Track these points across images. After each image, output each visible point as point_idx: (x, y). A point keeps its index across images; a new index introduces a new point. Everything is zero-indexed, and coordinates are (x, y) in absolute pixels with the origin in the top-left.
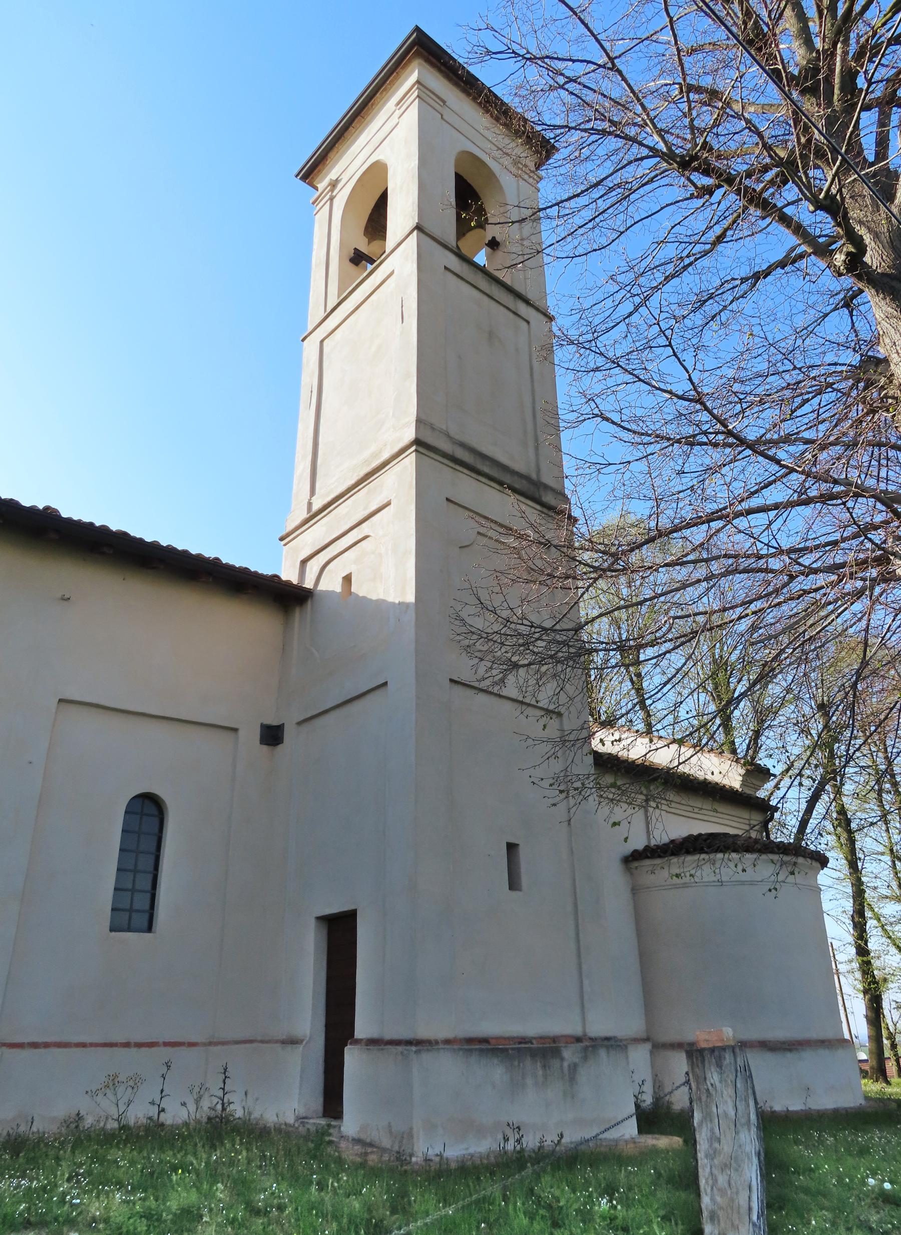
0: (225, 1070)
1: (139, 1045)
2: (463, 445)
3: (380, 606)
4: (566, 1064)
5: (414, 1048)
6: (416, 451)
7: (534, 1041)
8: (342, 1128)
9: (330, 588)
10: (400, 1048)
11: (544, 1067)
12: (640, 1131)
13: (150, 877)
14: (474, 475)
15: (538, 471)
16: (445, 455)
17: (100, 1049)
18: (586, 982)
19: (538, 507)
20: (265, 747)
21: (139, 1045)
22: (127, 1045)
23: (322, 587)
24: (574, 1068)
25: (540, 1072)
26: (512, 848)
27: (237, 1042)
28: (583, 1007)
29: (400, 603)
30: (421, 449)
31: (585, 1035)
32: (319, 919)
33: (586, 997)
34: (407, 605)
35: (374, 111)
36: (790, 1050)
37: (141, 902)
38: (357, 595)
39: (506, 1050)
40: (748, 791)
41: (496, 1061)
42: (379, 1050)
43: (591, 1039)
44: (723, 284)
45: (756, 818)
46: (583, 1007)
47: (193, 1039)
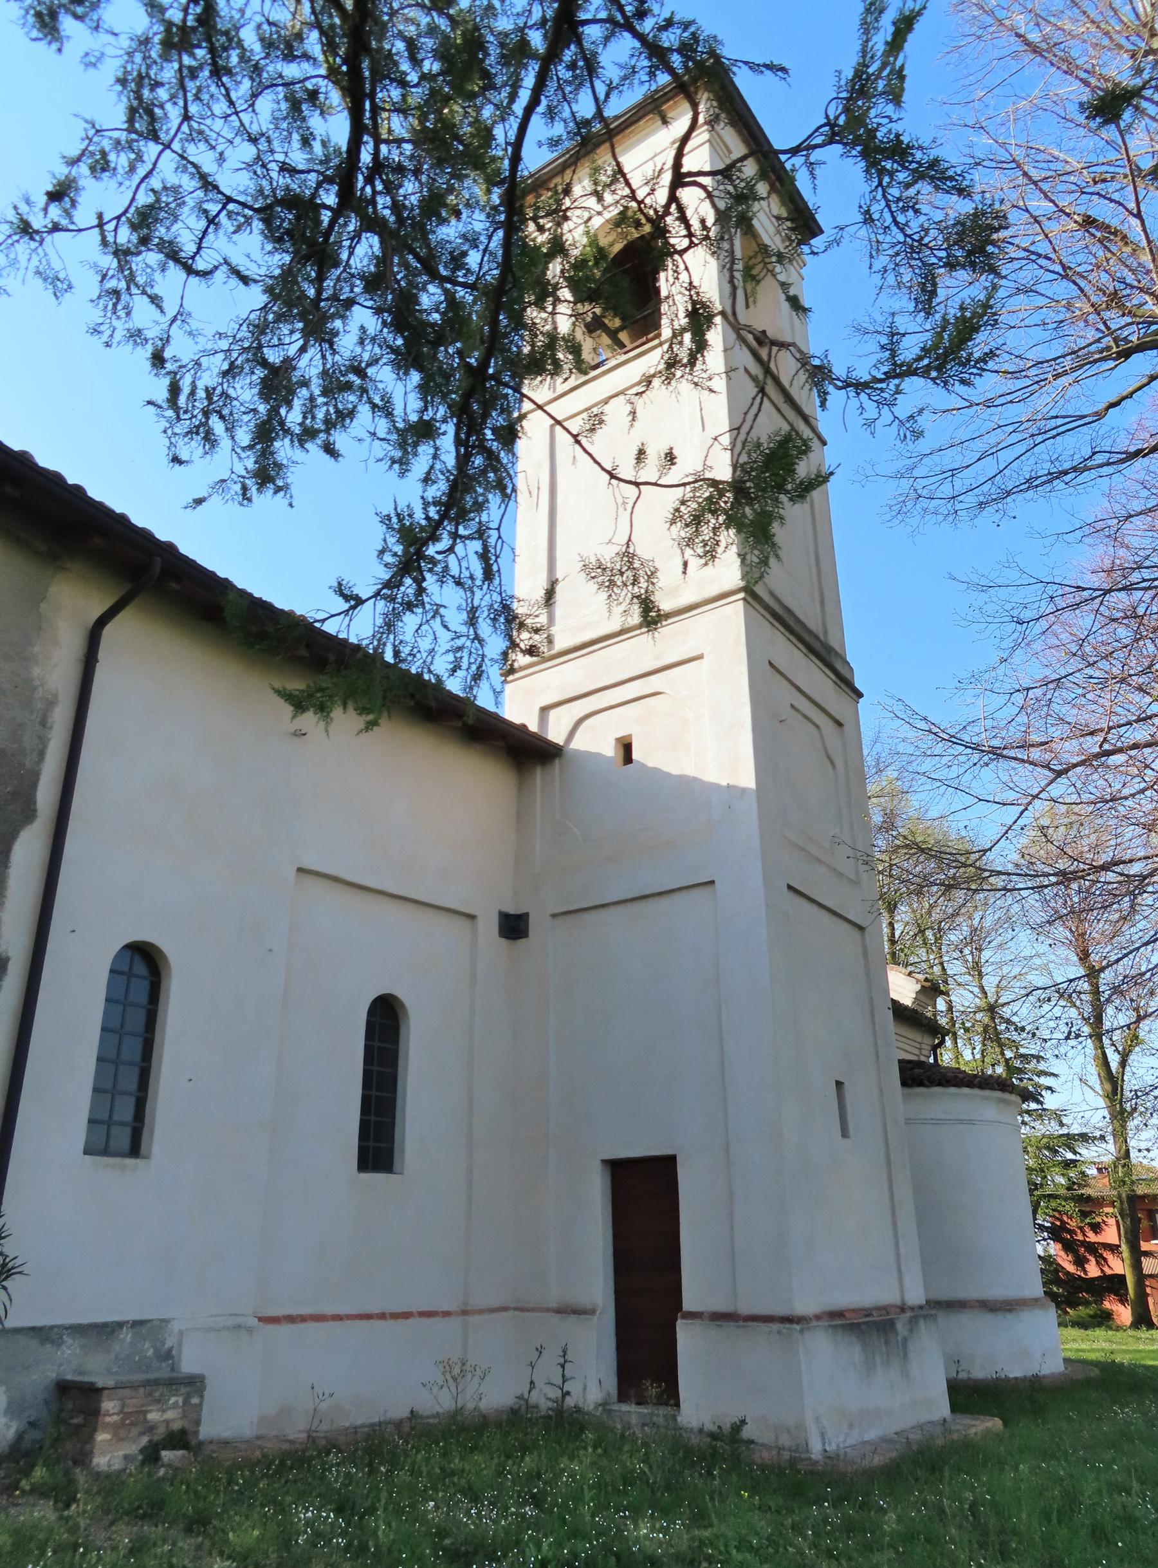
0: (565, 1352)
1: (396, 1316)
2: (772, 594)
3: (687, 787)
4: (899, 1338)
5: (798, 1327)
6: (744, 599)
7: (874, 1313)
8: (679, 1419)
9: (593, 748)
10: (775, 1326)
11: (886, 1343)
12: (954, 1408)
13: (135, 1073)
14: (787, 634)
15: (826, 632)
16: (767, 608)
17: (356, 1322)
18: (901, 1242)
19: (833, 677)
20: (503, 940)
21: (396, 1316)
22: (382, 1316)
23: (578, 744)
24: (905, 1340)
25: (884, 1349)
26: (839, 1084)
27: (493, 1310)
28: (900, 1271)
29: (728, 786)
30: (749, 599)
31: (904, 1303)
32: (604, 1162)
33: (902, 1260)
34: (744, 791)
35: (630, 141)
36: (1010, 1311)
37: (125, 1110)
38: (644, 766)
39: (858, 1325)
40: (919, 1009)
41: (854, 1338)
42: (738, 1327)
43: (912, 1309)
44: (1094, 453)
45: (928, 1041)
46: (900, 1271)
47: (446, 1307)
